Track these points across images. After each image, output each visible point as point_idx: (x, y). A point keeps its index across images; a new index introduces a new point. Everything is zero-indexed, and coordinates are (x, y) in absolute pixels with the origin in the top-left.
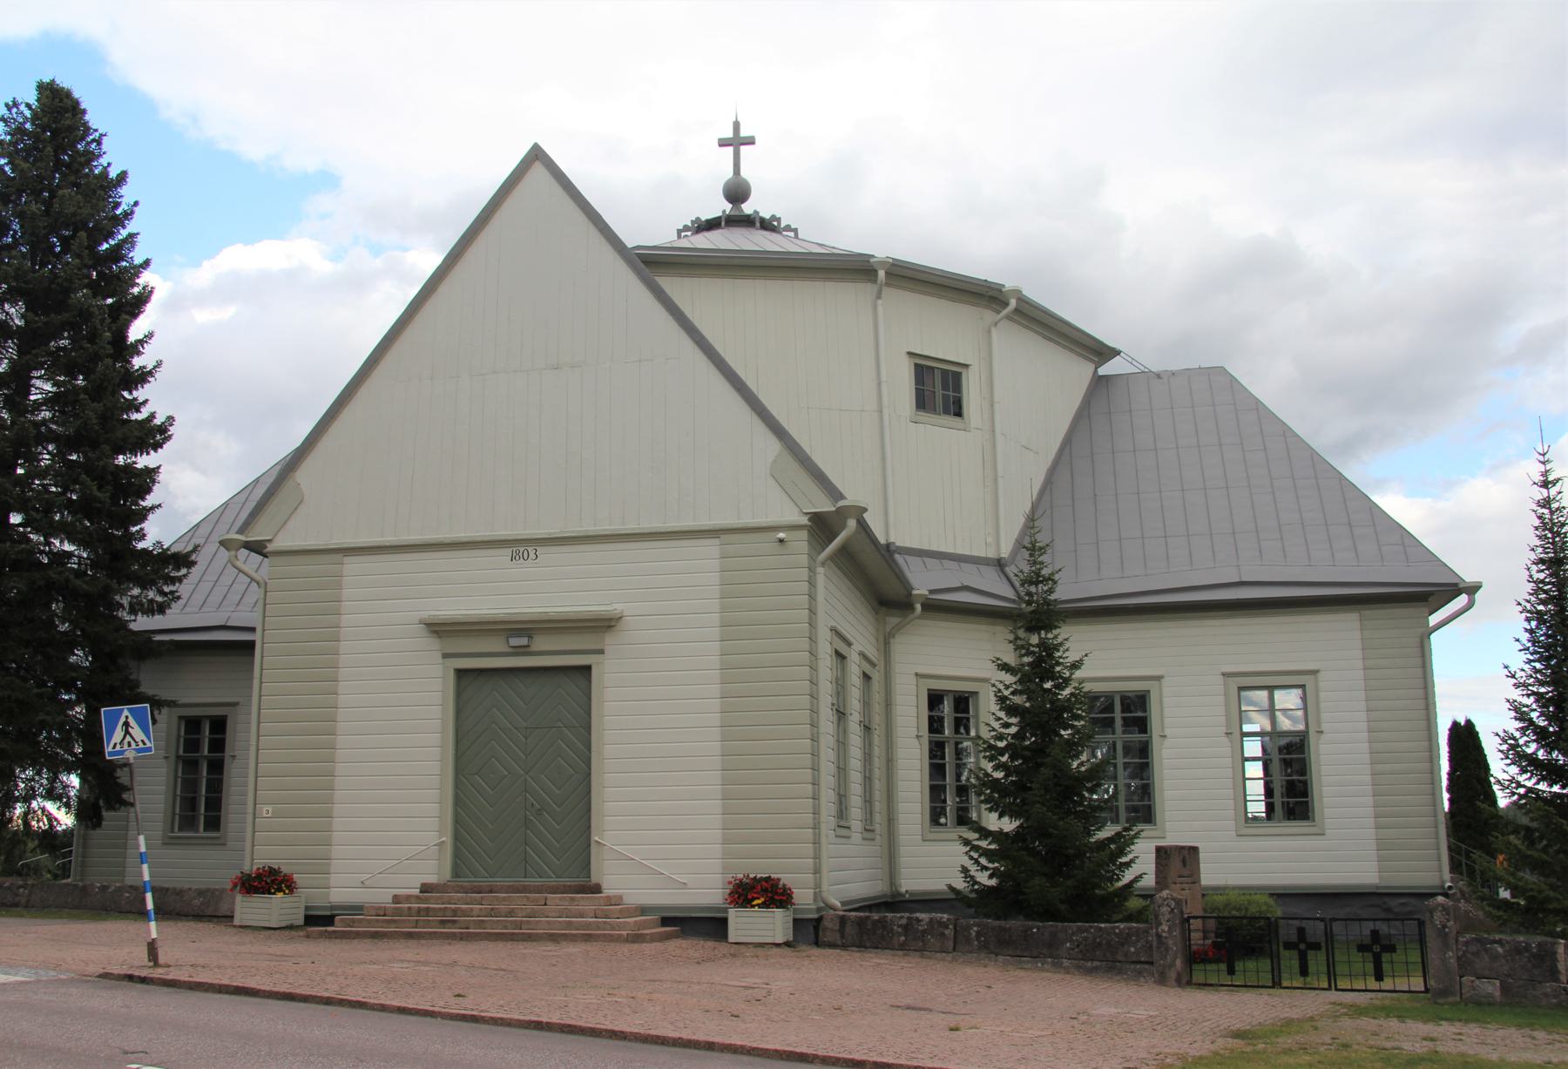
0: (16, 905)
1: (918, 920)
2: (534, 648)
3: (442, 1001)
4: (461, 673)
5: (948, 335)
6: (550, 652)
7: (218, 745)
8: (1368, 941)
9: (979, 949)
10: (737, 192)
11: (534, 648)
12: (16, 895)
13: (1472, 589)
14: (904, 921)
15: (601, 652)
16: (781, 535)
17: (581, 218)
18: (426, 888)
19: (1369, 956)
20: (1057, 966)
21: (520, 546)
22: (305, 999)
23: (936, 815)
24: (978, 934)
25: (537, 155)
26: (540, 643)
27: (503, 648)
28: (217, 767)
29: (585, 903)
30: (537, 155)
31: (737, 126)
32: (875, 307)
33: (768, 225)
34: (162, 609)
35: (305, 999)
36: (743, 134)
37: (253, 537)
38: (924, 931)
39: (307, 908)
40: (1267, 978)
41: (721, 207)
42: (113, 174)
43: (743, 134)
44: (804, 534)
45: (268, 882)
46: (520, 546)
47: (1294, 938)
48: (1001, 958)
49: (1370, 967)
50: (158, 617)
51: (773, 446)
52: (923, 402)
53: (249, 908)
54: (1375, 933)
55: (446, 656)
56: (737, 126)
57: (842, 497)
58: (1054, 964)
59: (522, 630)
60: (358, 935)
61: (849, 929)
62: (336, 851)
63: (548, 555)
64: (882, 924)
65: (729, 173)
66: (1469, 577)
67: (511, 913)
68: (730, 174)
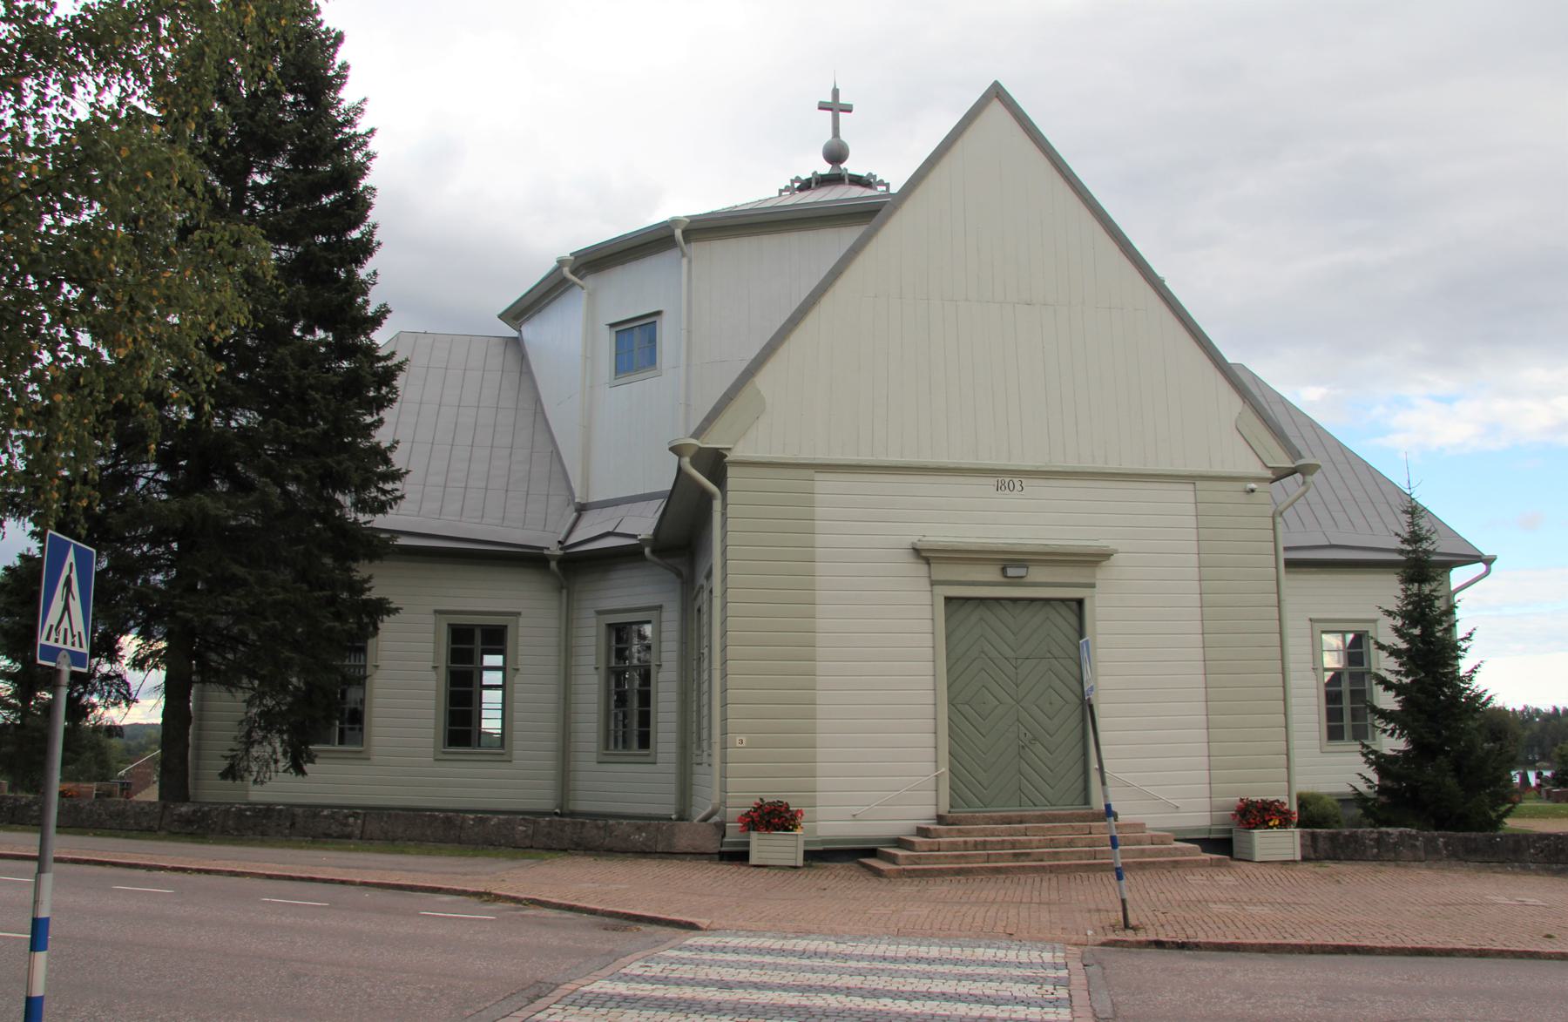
0: (349, 837)
1: (1388, 834)
2: (1029, 579)
3: (1242, 970)
4: (948, 600)
6: (1044, 583)
9: (1448, 857)
10: (836, 154)
12: (346, 825)
13: (1488, 561)
14: (1375, 836)
15: (1092, 586)
16: (1253, 486)
17: (1044, 163)
20: (1525, 870)
23: (1335, 734)
24: (1446, 845)
25: (997, 93)
26: (1037, 574)
29: (1101, 830)
30: (997, 93)
31: (836, 93)
33: (857, 181)
34: (382, 508)
36: (842, 100)
38: (1395, 844)
39: (806, 843)
41: (825, 168)
43: (842, 100)
45: (774, 817)
50: (380, 516)
51: (1236, 404)
52: (622, 329)
53: (764, 846)
55: (933, 583)
56: (836, 93)
57: (1301, 457)
58: (1523, 868)
59: (1010, 561)
60: (941, 873)
61: (1321, 844)
62: (821, 782)
64: (1329, 831)
65: (828, 136)
68: (828, 136)
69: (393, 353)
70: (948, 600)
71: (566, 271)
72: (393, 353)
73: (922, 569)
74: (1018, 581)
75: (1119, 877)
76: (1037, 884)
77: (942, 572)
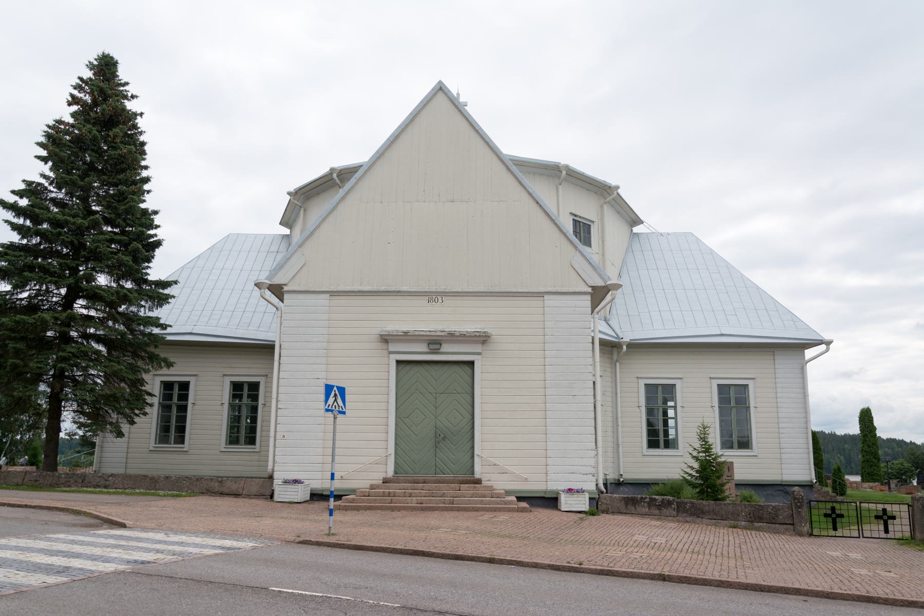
4: (399, 362)
5: (587, 208)
7: (255, 397)
8: (881, 514)
11: (442, 350)
13: (828, 343)
18: (386, 481)
19: (830, 519)
21: (433, 296)
22: (501, 562)
25: (441, 88)
27: (426, 350)
28: (183, 409)
30: (441, 88)
32: (557, 190)
35: (501, 562)
37: (277, 281)
40: (856, 534)
42: (75, 108)
44: (589, 297)
46: (433, 296)
47: (838, 512)
48: (705, 521)
49: (882, 527)
54: (884, 510)
59: (435, 343)
63: (448, 301)
66: (826, 336)
67: (443, 495)
69: (6, 221)
70: (399, 362)
71: (335, 176)
72: (6, 221)
73: (384, 346)
74: (435, 352)
75: (331, 514)
76: (708, 532)
77: (392, 347)
